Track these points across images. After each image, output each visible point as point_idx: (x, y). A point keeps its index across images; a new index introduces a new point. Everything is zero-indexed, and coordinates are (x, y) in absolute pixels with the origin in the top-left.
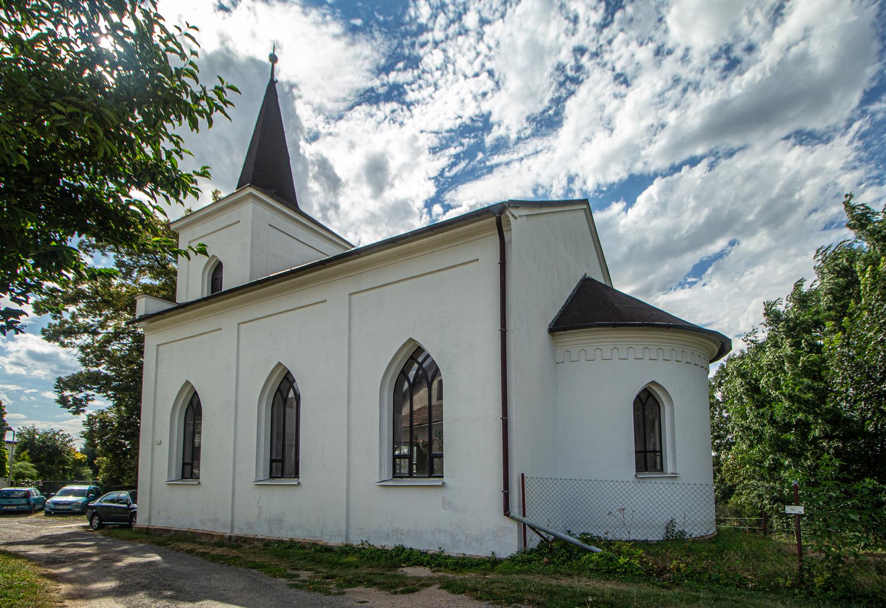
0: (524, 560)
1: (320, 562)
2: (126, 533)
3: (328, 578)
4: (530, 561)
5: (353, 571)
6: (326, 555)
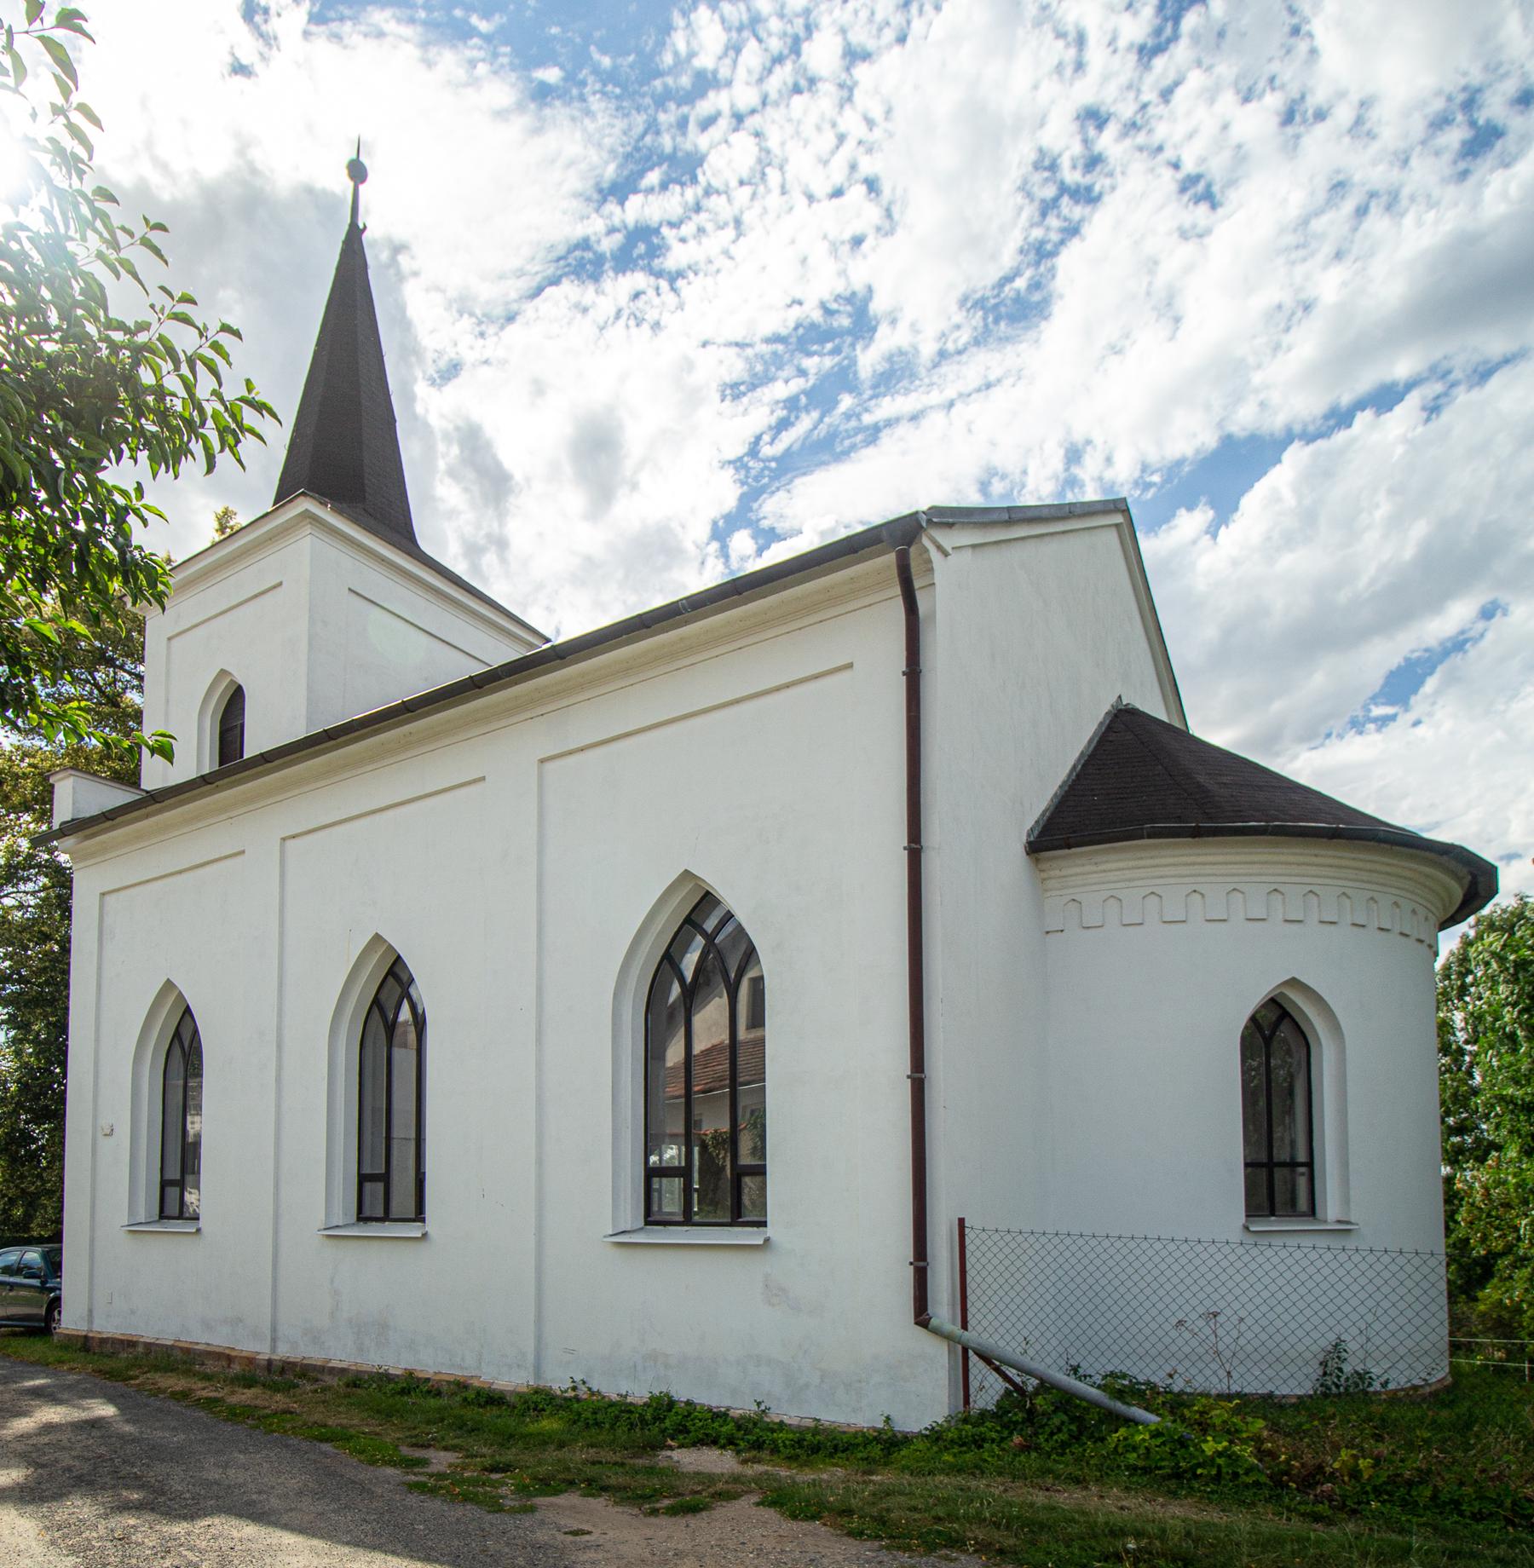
0: (964, 1439)
6: (490, 1413)
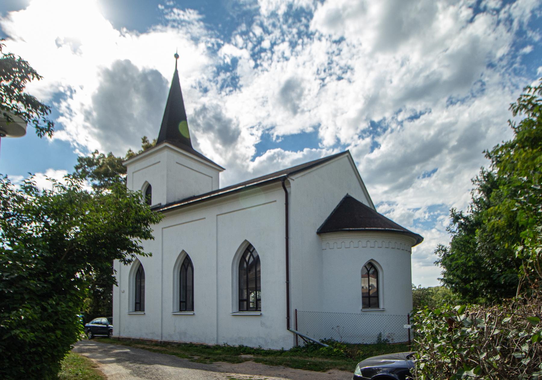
0: (296, 350)
1: (204, 353)
2: (107, 340)
3: (206, 358)
4: (297, 351)
5: (218, 356)
6: (207, 350)
